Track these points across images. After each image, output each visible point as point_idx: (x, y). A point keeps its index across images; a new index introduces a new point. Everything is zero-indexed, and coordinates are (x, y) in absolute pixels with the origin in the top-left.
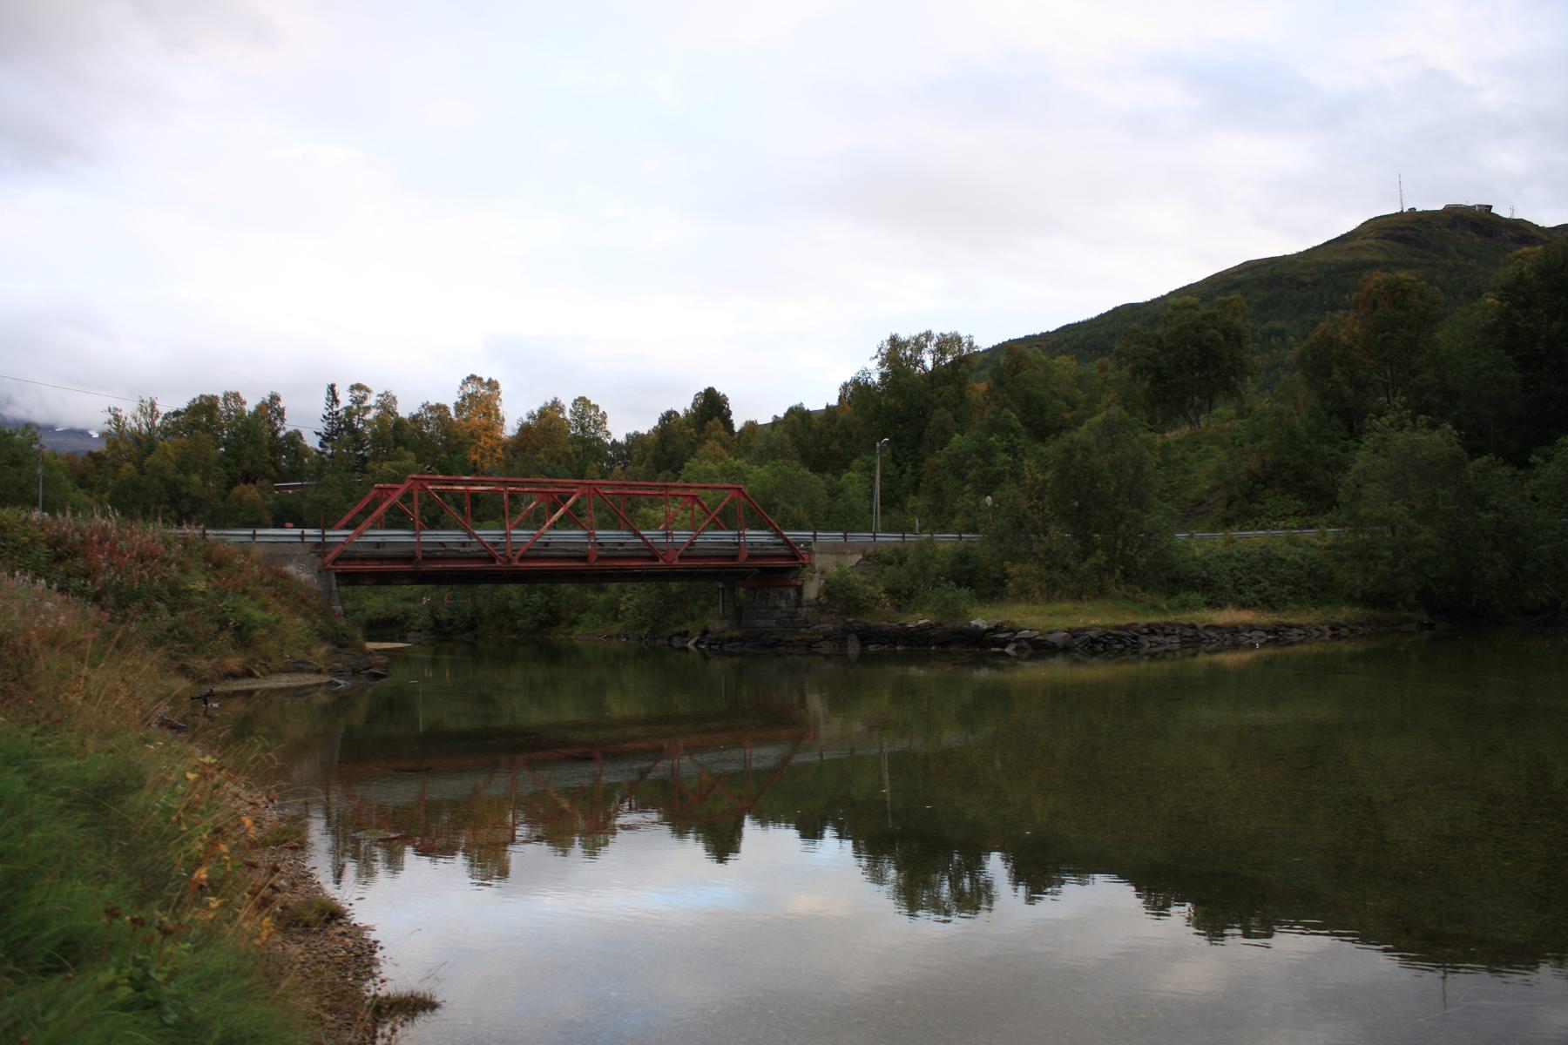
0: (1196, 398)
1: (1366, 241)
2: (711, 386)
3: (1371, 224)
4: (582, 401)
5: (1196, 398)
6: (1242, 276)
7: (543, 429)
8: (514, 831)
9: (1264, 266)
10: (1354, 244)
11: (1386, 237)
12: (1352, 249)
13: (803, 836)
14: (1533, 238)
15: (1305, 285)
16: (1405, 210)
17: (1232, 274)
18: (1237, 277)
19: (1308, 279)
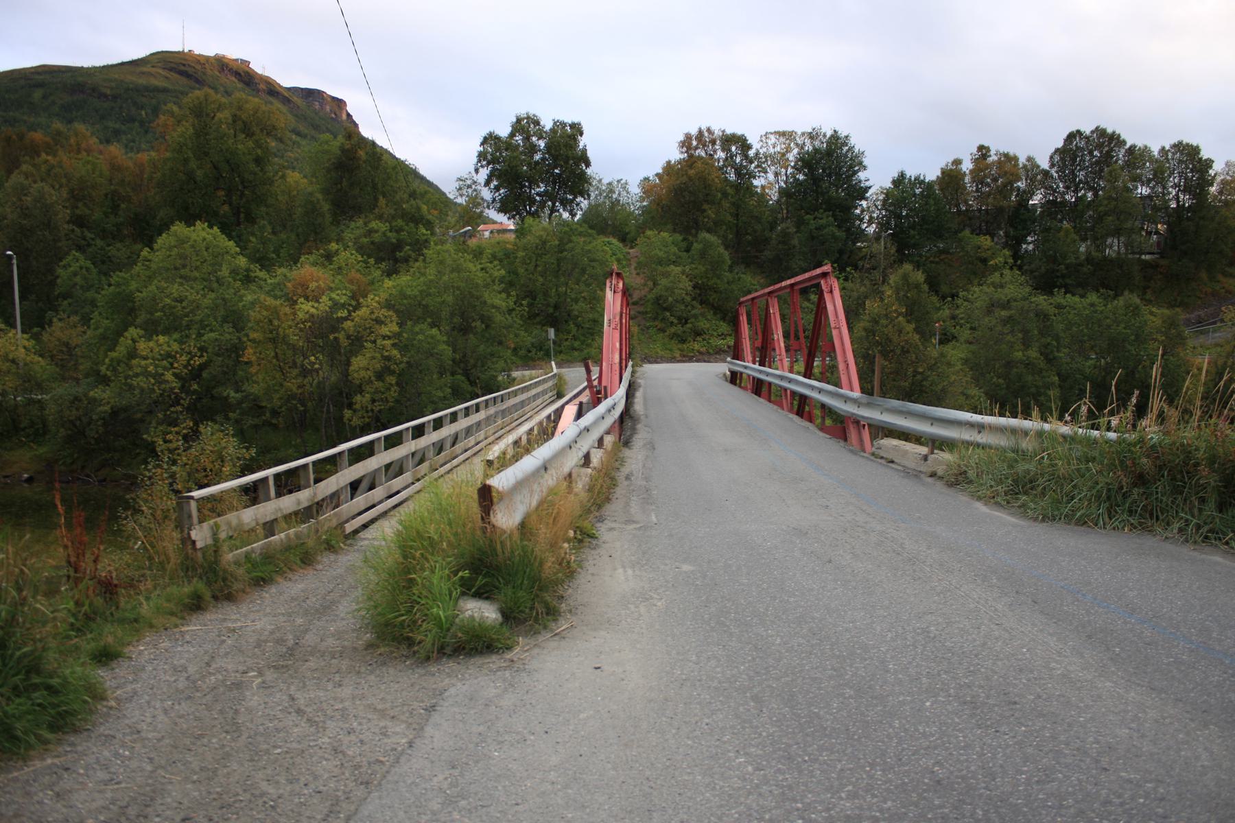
0: (703, 154)
1: (154, 69)
2: (956, 157)
3: (159, 56)
4: (1029, 159)
5: (703, 154)
6: (41, 77)
7: (592, 334)
8: (348, 364)
9: (63, 72)
10: (144, 69)
11: (171, 70)
12: (143, 73)
13: (1107, 141)
14: (278, 93)
15: (106, 96)
16: (186, 51)
17: (32, 73)
18: (37, 77)
19: (108, 92)
